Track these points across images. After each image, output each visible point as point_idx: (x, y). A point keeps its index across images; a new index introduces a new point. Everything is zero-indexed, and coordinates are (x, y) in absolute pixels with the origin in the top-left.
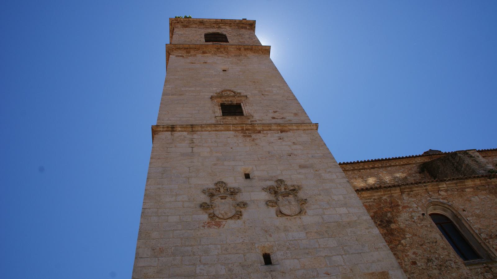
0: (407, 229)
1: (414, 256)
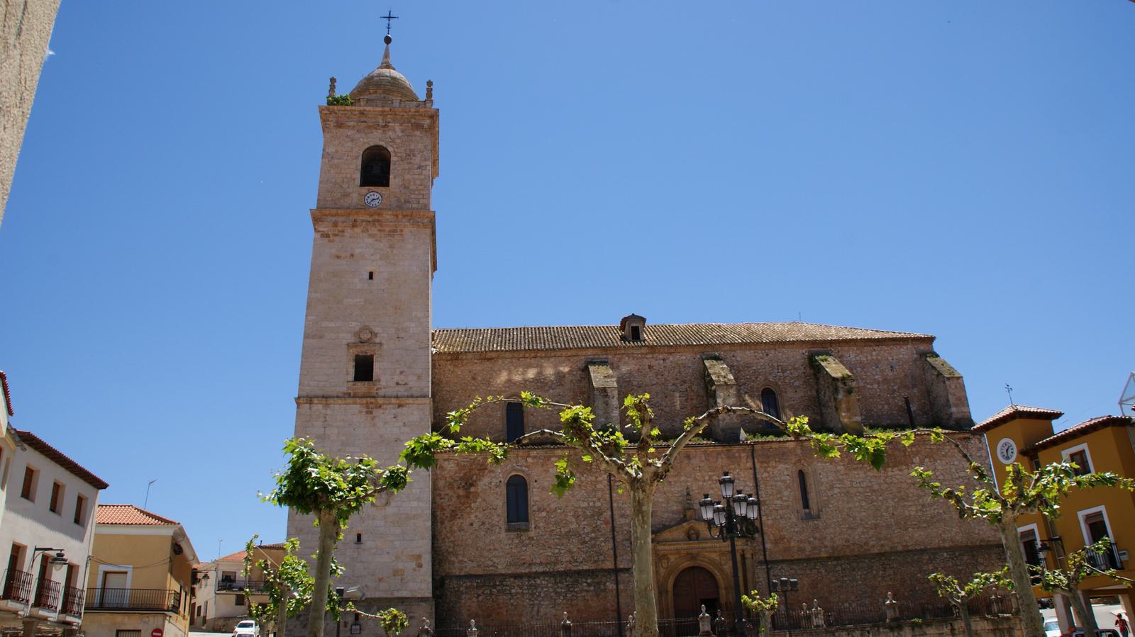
0: (481, 494)
1: (474, 518)
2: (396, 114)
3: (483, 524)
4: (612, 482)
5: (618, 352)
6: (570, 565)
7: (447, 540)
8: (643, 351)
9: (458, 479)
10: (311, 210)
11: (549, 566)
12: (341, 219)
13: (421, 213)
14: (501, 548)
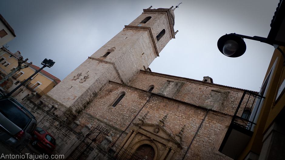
10: (143, 9)
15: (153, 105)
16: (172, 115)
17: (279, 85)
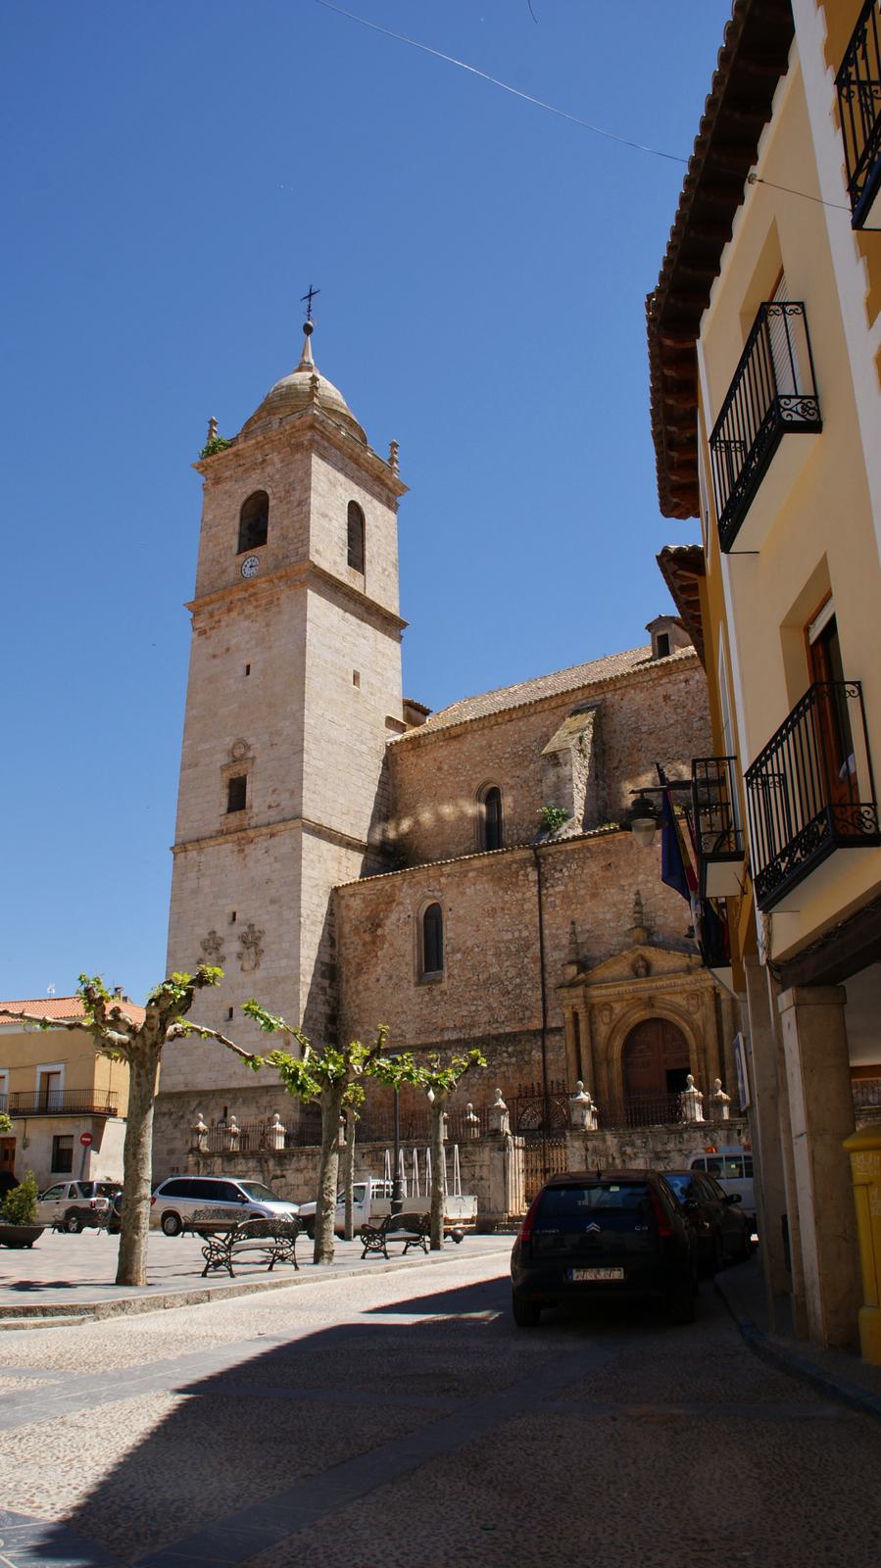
0: (388, 937)
2: (272, 441)
3: (391, 978)
4: (544, 898)
5: (618, 685)
6: (488, 1028)
7: (352, 1004)
8: (654, 675)
9: (364, 920)
11: (464, 1031)
12: (217, 606)
13: (296, 568)
14: (410, 1009)
15: (570, 888)
16: (650, 885)
17: (822, 946)
